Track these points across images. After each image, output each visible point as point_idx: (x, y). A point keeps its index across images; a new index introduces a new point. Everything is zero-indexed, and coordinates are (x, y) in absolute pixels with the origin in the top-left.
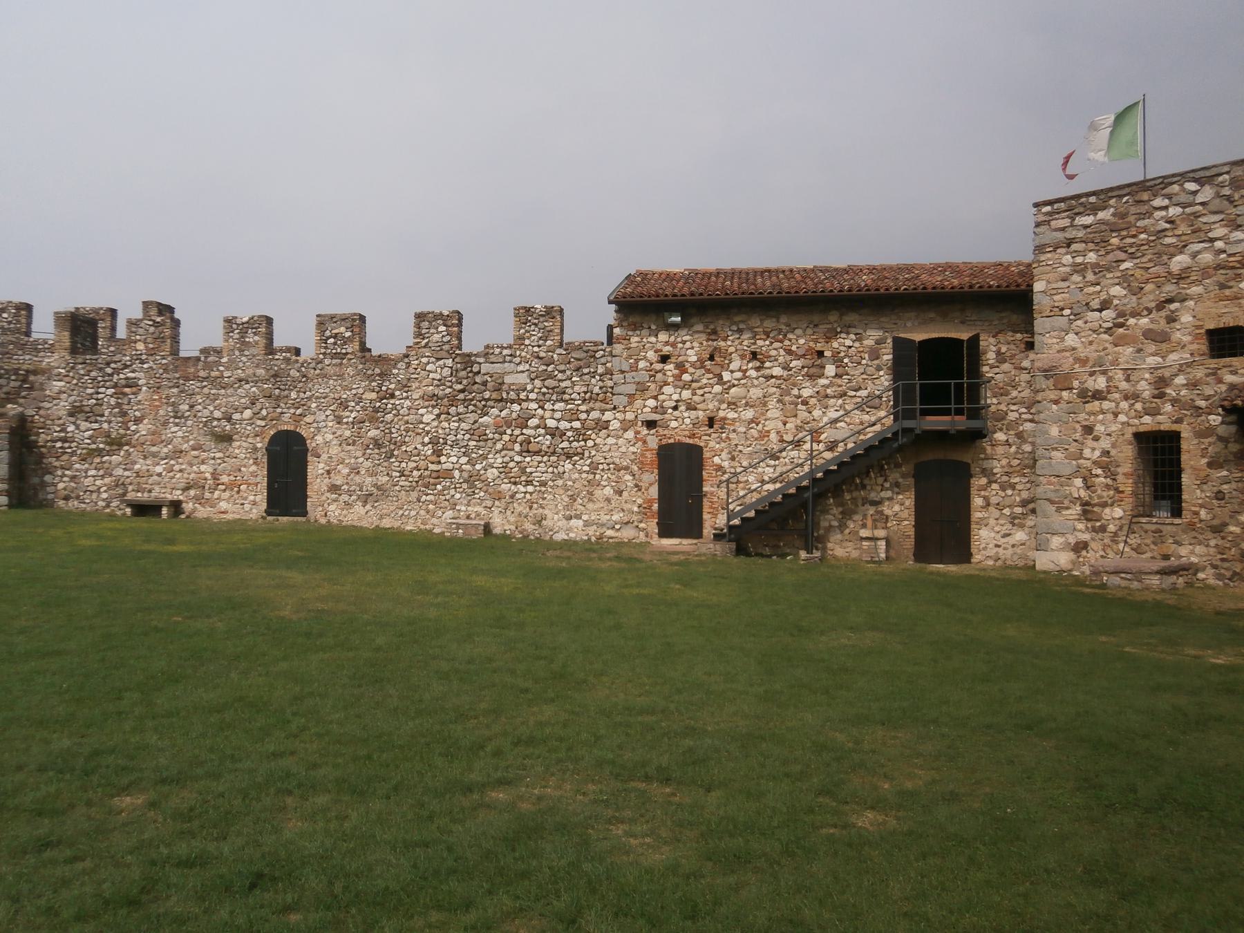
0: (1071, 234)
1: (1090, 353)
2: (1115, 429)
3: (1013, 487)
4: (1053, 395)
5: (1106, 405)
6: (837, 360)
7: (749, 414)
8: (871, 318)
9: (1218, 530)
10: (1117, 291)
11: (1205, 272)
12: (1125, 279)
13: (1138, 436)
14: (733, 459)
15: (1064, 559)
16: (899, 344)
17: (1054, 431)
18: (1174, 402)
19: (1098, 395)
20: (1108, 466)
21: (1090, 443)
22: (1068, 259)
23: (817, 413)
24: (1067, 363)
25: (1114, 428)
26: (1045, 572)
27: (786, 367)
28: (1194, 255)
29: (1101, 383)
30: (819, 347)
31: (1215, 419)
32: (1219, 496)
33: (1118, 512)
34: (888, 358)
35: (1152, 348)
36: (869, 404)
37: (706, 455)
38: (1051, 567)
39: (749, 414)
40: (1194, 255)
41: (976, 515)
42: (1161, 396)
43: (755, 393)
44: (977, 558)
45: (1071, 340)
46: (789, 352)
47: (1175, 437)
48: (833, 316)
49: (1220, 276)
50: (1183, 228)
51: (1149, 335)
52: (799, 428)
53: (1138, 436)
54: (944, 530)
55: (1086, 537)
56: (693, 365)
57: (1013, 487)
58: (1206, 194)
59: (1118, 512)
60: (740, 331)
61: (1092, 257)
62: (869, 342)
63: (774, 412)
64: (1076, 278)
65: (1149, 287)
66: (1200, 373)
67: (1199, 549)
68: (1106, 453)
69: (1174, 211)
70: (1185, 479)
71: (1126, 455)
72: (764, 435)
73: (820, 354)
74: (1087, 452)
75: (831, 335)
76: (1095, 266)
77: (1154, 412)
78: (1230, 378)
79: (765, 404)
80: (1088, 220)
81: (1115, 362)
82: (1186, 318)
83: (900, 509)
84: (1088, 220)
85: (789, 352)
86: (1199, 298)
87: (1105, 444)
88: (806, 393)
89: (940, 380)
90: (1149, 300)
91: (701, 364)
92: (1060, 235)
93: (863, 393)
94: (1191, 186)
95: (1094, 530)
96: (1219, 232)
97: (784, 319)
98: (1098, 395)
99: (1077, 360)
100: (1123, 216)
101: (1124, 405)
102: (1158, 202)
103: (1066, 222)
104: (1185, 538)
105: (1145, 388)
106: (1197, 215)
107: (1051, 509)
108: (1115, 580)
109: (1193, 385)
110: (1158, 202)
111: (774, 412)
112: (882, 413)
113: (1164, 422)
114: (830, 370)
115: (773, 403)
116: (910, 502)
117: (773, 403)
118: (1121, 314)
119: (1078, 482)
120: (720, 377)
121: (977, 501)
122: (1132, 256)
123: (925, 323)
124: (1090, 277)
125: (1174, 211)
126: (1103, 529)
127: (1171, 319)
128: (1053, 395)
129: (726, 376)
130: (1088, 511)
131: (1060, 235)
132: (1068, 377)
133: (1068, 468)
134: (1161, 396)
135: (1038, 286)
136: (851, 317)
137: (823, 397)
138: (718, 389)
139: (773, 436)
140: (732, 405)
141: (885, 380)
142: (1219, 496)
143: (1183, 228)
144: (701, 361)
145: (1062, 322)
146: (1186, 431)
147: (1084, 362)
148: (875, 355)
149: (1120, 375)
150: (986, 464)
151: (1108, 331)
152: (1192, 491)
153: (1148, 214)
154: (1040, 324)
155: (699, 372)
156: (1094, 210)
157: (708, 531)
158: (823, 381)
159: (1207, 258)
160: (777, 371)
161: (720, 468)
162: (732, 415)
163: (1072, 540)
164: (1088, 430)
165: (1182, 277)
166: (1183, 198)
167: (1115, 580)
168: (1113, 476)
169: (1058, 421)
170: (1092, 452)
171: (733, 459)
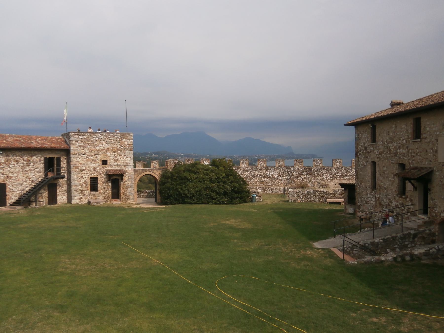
0: (78, 139)
1: (82, 162)
2: (87, 177)
3: (63, 187)
4: (75, 170)
5: (85, 172)
6: (33, 162)
7: (16, 175)
8: (300, 207)
9: (104, 194)
10: (87, 151)
11: (102, 150)
12: (88, 149)
13: (91, 178)
14: (12, 186)
15: (78, 201)
16: (45, 159)
17: (75, 177)
18: (97, 172)
19: (83, 170)
20: (85, 183)
21: (82, 179)
22: (78, 144)
23: (29, 174)
24: (78, 164)
25: (87, 176)
26: (74, 204)
27: (23, 164)
28: (100, 147)
29: (84, 168)
30: (30, 159)
31: (103, 175)
32: (104, 188)
33: (88, 192)
34: (42, 161)
35: (93, 162)
36: (39, 172)
37: (7, 185)
38: (75, 203)
39: (16, 175)
40: (100, 147)
41: (58, 194)
42: (95, 171)
43: (17, 170)
44: (58, 203)
45: (78, 159)
46: (24, 160)
47: (97, 178)
48: (32, 152)
49: (104, 151)
50: (98, 142)
51: (93, 160)
52: (26, 178)
53: (91, 178)
54: (53, 199)
55: (82, 196)
56: (3, 163)
57: (63, 187)
58: (102, 137)
59: (88, 192)
60: (13, 155)
61: (82, 144)
62: (39, 158)
63: (21, 174)
64: (79, 148)
65: (93, 151)
66: (101, 167)
67: (101, 197)
68: (85, 181)
69: (97, 139)
70: (99, 185)
71: (89, 181)
72: (19, 180)
73: (30, 160)
74: (82, 181)
75: (32, 156)
76: (83, 146)
77: (94, 174)
78: (105, 168)
79: (19, 172)
80: (82, 137)
81: (87, 164)
82: (99, 158)
83: (45, 194)
84: (82, 137)
85: (24, 160)
86: (100, 154)
87: (85, 179)
88: (27, 169)
89: (50, 164)
90: (93, 154)
91: (5, 163)
92: (76, 139)
93: (38, 169)
94: (100, 135)
95: (83, 195)
96: (104, 144)
97: (23, 152)
98: (83, 170)
99: (80, 163)
100: (88, 138)
101: (88, 172)
102: (94, 137)
103: (77, 137)
104: (99, 195)
105: (92, 169)
106: (100, 140)
107: (75, 192)
108: (95, 204)
109: (100, 169)
110: (94, 137)
111: (21, 174)
112: (42, 174)
113: (95, 175)
114: (32, 164)
115: (21, 172)
116: (47, 193)
117: (21, 172)
118: (88, 156)
119: (80, 186)
120: (9, 166)
121: (58, 191)
122: (90, 145)
123: (49, 154)
124: (82, 148)
125: (97, 139)
126: (85, 195)
127: (96, 158)
128: (75, 170)
129: (11, 166)
130: (82, 192)
131: (76, 139)
132: (78, 167)
133: (78, 184)
134: (95, 171)
135: (72, 148)
136: (36, 152)
137: (30, 170)
138: (9, 169)
139: (21, 180)
140: (12, 173)
141: (42, 166)
142: (104, 188)
143: (98, 142)
144: (5, 162)
145: (77, 156)
146: (99, 177)
147: (81, 164)
148: (40, 160)
149: (88, 167)
150: (59, 183)
151: (85, 158)
152: (100, 187)
153: (92, 138)
154: (72, 156)
155: (4, 165)
156: (83, 135)
157: (8, 204)
158: (31, 167)
159: (102, 148)
160: (21, 165)
161: (10, 189)
162: (12, 175)
163: (79, 197)
164: (82, 177)
165: (98, 150)
166: (99, 137)
167: (95, 204)
168: (86, 185)
169: (76, 175)
170: (83, 181)
171: (12, 186)
